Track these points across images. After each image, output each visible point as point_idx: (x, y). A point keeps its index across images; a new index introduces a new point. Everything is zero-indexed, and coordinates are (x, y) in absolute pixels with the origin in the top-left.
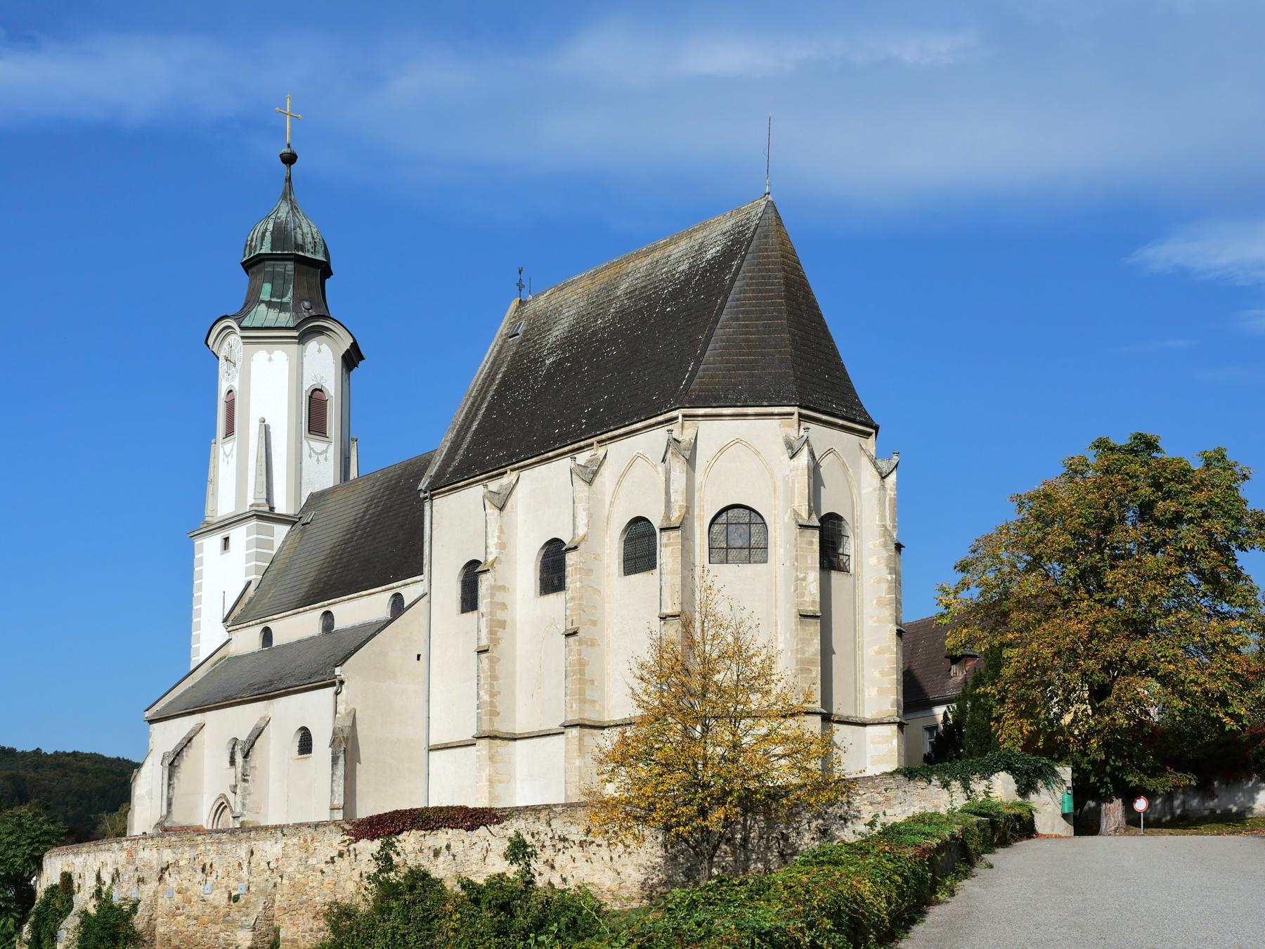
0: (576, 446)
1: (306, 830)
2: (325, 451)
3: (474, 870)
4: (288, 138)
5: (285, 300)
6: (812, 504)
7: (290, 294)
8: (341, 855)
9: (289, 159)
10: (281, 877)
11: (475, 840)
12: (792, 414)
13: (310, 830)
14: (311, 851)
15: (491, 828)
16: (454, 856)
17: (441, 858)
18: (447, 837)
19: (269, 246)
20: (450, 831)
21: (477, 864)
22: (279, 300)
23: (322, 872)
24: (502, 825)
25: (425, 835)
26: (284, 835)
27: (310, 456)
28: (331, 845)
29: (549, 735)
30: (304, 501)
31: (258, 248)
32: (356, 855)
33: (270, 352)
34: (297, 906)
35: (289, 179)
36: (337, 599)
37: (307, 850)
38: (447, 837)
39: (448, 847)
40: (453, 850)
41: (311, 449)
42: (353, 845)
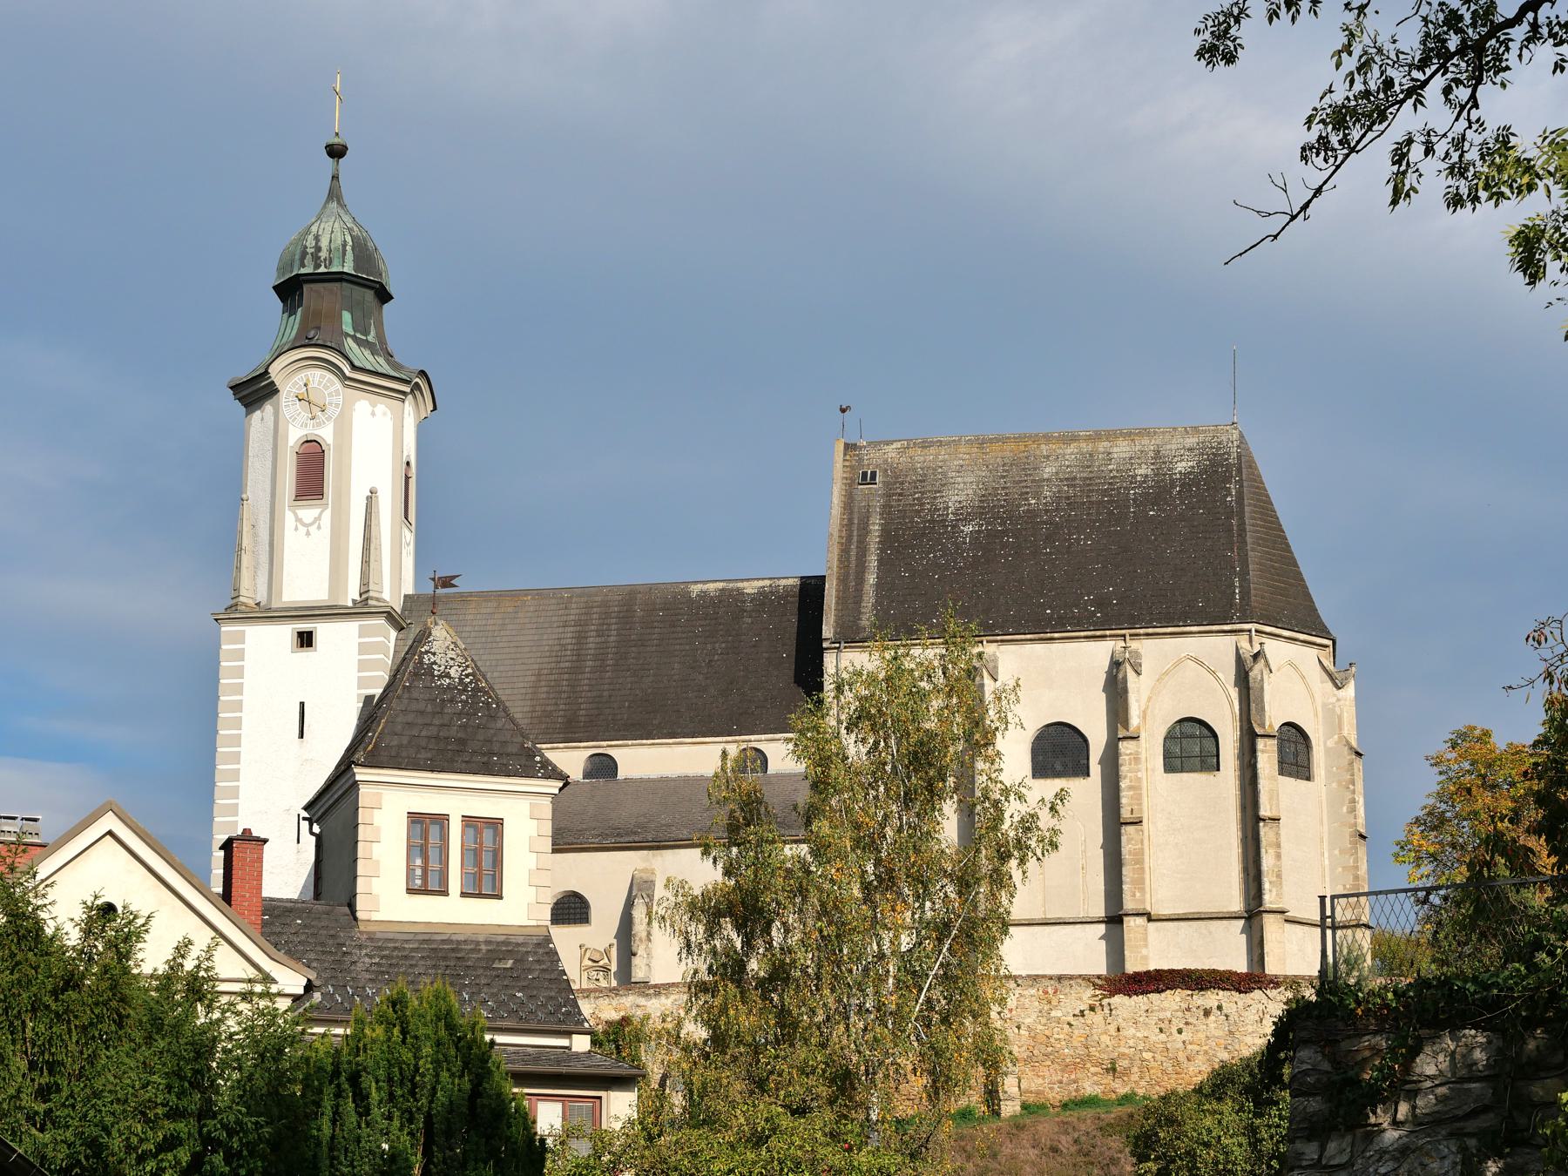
0: (1098, 633)
1: (1047, 982)
2: (318, 518)
3: (1250, 1031)
4: (337, 126)
8: (1092, 1009)
10: (1019, 1027)
11: (1251, 1002)
12: (1327, 646)
13: (1052, 982)
14: (1054, 1002)
15: (1268, 992)
16: (1227, 1016)
17: (1212, 1018)
18: (1217, 998)
20: (1221, 993)
21: (1252, 1025)
23: (1070, 1025)
24: (1279, 990)
25: (1192, 995)
26: (1018, 985)
27: (296, 529)
28: (1081, 999)
29: (1065, 923)
31: (336, 261)
32: (1111, 1010)
33: (374, 405)
34: (1041, 1057)
35: (335, 177)
36: (630, 742)
37: (1050, 1002)
38: (1217, 998)
39: (1220, 1008)
40: (1225, 1011)
41: (298, 520)
42: (1105, 1002)
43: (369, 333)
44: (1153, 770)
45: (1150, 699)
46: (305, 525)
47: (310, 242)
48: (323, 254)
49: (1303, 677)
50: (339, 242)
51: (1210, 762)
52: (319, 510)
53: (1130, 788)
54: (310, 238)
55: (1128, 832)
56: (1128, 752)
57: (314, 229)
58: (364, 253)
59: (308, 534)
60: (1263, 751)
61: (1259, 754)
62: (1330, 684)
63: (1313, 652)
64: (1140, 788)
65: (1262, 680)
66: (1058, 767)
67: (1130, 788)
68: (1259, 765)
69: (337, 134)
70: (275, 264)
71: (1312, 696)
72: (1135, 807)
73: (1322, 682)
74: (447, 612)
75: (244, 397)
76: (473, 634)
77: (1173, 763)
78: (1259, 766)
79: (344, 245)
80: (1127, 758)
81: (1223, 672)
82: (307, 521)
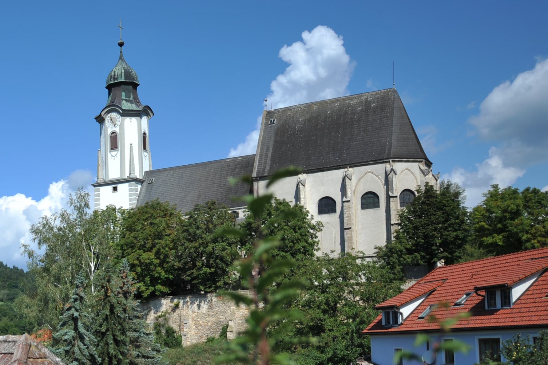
2: (116, 154)
5: (131, 99)
6: (228, 160)
7: (132, 96)
9: (121, 45)
12: (423, 161)
19: (124, 78)
22: (129, 99)
30: (143, 174)
31: (119, 78)
35: (121, 52)
41: (112, 155)
43: (130, 97)
44: (357, 209)
45: (356, 186)
46: (114, 157)
47: (113, 74)
48: (116, 77)
49: (412, 173)
50: (120, 72)
51: (376, 205)
52: (116, 152)
53: (347, 217)
54: (113, 72)
55: (346, 232)
56: (346, 205)
57: (114, 69)
58: (128, 74)
59: (114, 159)
60: (392, 202)
61: (391, 203)
62: (422, 174)
63: (416, 164)
64: (350, 217)
65: (392, 178)
66: (327, 210)
67: (347, 217)
68: (391, 206)
69: (121, 39)
70: (106, 81)
71: (416, 179)
72: (349, 223)
73: (420, 173)
74: (155, 175)
75: (99, 120)
76: (162, 182)
77: (364, 206)
78: (391, 206)
79: (122, 72)
80: (346, 207)
81: (380, 175)
82: (114, 155)
